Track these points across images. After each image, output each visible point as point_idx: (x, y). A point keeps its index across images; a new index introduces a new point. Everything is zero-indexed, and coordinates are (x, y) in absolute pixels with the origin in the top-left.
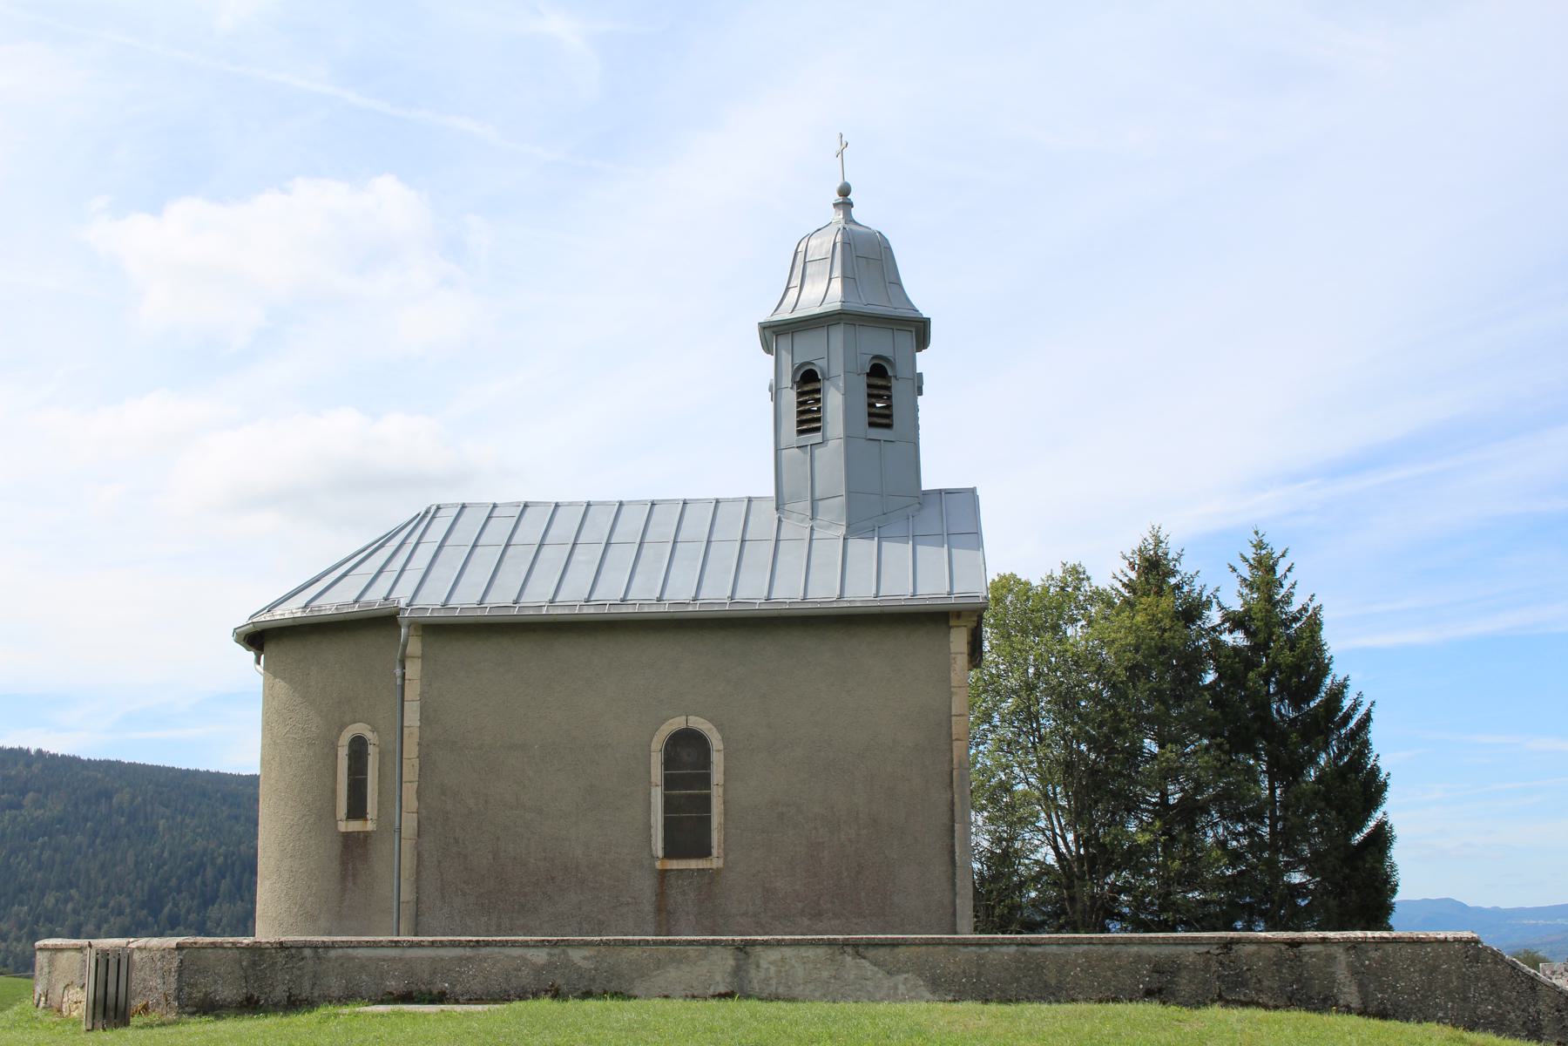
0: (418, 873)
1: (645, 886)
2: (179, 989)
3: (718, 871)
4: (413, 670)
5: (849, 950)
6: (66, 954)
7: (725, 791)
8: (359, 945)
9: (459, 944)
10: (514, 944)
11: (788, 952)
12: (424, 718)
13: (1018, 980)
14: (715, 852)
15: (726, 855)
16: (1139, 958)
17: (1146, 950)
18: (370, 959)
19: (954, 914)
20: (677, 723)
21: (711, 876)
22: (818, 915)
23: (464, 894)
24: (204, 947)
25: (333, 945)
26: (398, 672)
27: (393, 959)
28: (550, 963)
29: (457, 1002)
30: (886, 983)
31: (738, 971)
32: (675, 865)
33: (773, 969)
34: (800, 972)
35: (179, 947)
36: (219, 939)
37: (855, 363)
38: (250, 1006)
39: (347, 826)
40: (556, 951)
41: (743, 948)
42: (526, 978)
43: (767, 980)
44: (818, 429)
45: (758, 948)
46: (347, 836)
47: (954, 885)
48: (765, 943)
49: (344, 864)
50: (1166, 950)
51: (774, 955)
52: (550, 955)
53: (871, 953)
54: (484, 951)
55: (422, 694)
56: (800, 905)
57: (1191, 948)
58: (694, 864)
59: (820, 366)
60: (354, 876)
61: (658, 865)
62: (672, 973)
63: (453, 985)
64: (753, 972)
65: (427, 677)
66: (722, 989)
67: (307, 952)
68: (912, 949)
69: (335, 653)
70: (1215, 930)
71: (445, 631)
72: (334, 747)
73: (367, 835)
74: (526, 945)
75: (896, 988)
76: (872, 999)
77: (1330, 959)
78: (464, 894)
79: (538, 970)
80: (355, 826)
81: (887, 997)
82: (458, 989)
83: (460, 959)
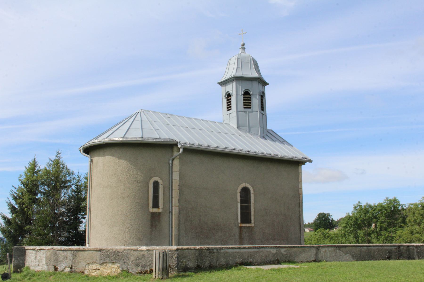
0: (179, 226)
1: (237, 230)
3: (253, 227)
4: (176, 162)
6: (86, 253)
8: (230, 248)
9: (255, 248)
10: (268, 247)
11: (326, 249)
14: (252, 222)
15: (255, 223)
16: (386, 249)
18: (232, 252)
19: (301, 240)
21: (251, 228)
22: (274, 240)
23: (192, 233)
24: (185, 249)
26: (171, 162)
27: (238, 253)
28: (276, 253)
29: (254, 265)
31: (316, 254)
33: (323, 254)
35: (177, 250)
36: (189, 247)
37: (249, 92)
38: (198, 269)
39: (152, 210)
40: (278, 249)
41: (318, 248)
42: (271, 257)
44: (250, 108)
46: (153, 213)
47: (301, 232)
48: (323, 247)
49: (152, 222)
52: (276, 250)
55: (180, 170)
59: (231, 92)
60: (155, 226)
61: (239, 225)
63: (253, 260)
64: (319, 254)
65: (181, 164)
66: (313, 259)
67: (215, 251)
68: (349, 248)
69: (147, 154)
71: (190, 151)
72: (148, 184)
73: (160, 213)
74: (271, 248)
77: (414, 249)
78: (192, 233)
79: (274, 255)
80: (155, 210)
81: (345, 260)
82: (255, 261)
83: (255, 252)
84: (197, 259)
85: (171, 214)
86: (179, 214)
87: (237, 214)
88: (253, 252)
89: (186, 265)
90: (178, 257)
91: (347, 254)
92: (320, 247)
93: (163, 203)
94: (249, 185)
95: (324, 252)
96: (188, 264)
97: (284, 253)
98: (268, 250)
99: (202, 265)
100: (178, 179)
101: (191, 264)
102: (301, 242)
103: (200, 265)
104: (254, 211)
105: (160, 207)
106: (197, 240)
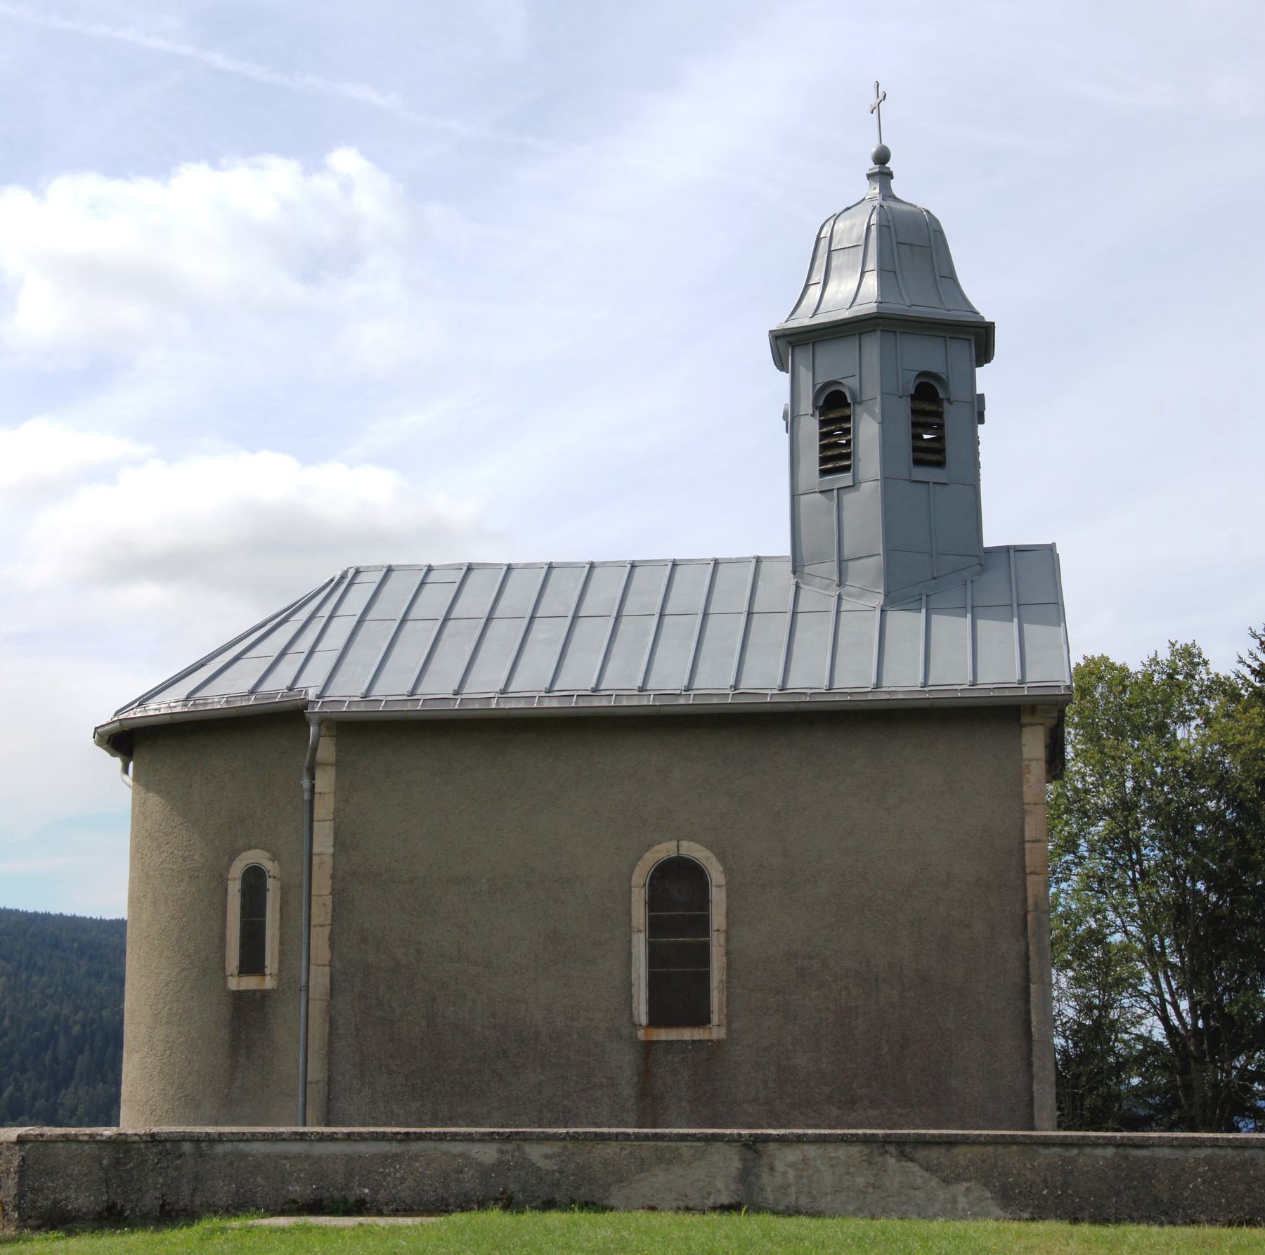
0: (331, 1043)
1: (624, 1062)
3: (719, 1043)
4: (325, 781)
5: (891, 1149)
7: (728, 939)
9: (383, 1137)
10: (454, 1137)
11: (812, 1151)
12: (341, 844)
14: (715, 1018)
15: (729, 1023)
18: (268, 1156)
19: (1031, 1104)
21: (711, 1049)
25: (221, 1138)
26: (306, 783)
27: (296, 1157)
29: (380, 1213)
31: (746, 1176)
32: (663, 1035)
33: (791, 1174)
35: (21, 1141)
37: (895, 379)
39: (234, 984)
40: (509, 1147)
41: (752, 1146)
43: (784, 1188)
44: (846, 469)
45: (772, 1146)
46: (239, 996)
47: (1030, 1064)
48: (781, 1139)
51: (793, 1154)
52: (501, 1152)
53: (921, 1154)
54: (415, 1147)
55: (336, 812)
56: (826, 1090)
58: (687, 1034)
61: (641, 1035)
64: (765, 1178)
65: (344, 790)
66: (725, 1199)
67: (187, 1147)
71: (374, 733)
72: (223, 881)
73: (265, 994)
74: (469, 1138)
76: (923, 1215)
79: (485, 1172)
80: (250, 983)
82: (382, 1196)
83: (385, 1156)
84: (107, 1181)
85: (303, 993)
86: (331, 996)
87: (630, 986)
88: (373, 1156)
89: (55, 1202)
90: (23, 1171)
91: (958, 1179)
92: (767, 1139)
93: (282, 953)
94: (697, 846)
95: (793, 1165)
96: (68, 1198)
97: (542, 1163)
98: (458, 1148)
99: (129, 1206)
100: (331, 850)
101: (80, 1200)
102: (1031, 1117)
103: (120, 1203)
104: (729, 967)
105: (267, 971)
106: (415, 1105)
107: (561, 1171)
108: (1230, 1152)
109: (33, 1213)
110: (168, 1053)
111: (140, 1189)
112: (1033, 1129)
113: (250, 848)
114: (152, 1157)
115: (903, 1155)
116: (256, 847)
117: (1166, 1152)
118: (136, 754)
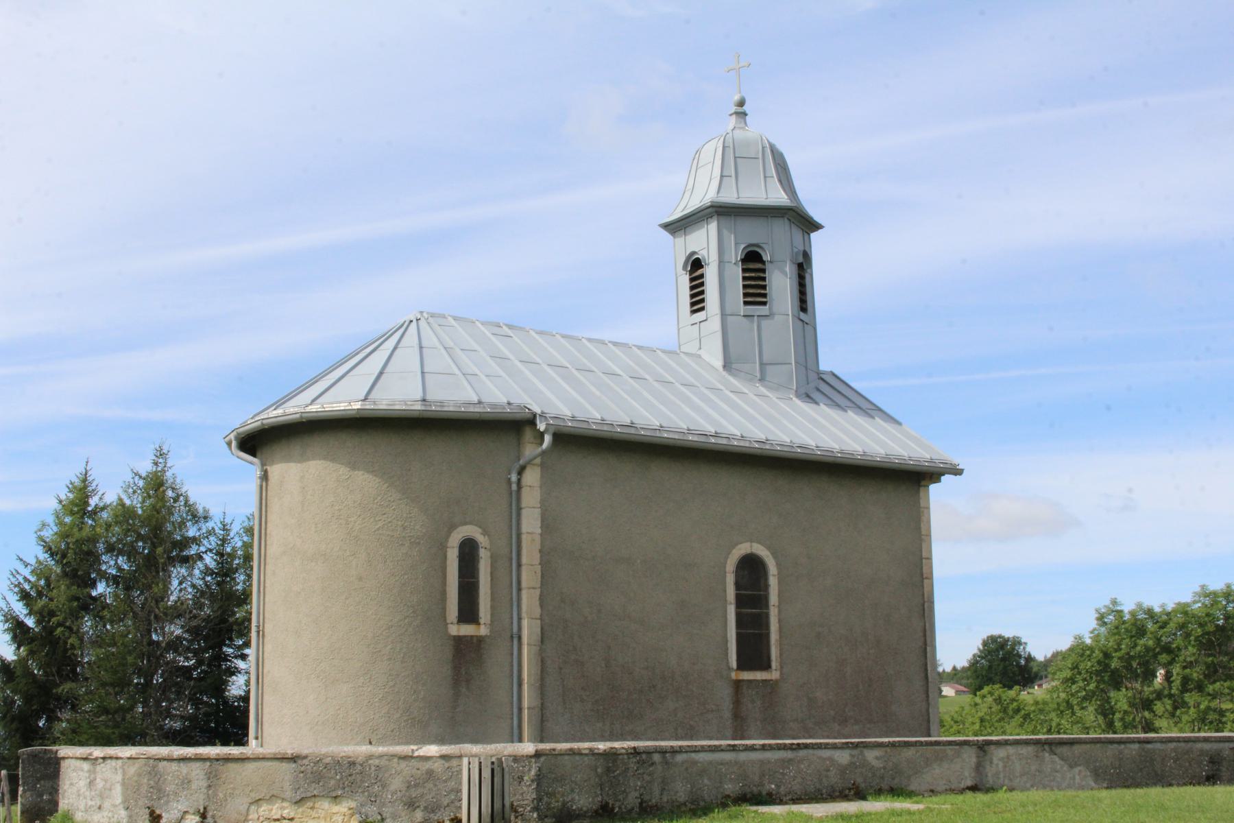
0: (542, 679)
1: (724, 694)
2: (539, 799)
3: (777, 681)
4: (532, 477)
5: (1046, 747)
7: (780, 612)
13: (1141, 770)
14: (774, 664)
15: (782, 667)
17: (1207, 746)
18: (710, 763)
19: (929, 721)
20: (743, 549)
22: (844, 721)
25: (680, 750)
26: (514, 478)
27: (728, 763)
29: (781, 802)
30: (1069, 775)
31: (979, 767)
32: (747, 676)
34: (1018, 767)
36: (575, 745)
37: (760, 252)
39: (456, 630)
40: (855, 752)
41: (983, 747)
42: (834, 778)
43: (997, 774)
44: (764, 303)
45: (993, 747)
46: (458, 640)
49: (457, 668)
50: (1216, 746)
51: (1001, 753)
52: (852, 756)
53: (1060, 750)
54: (802, 753)
55: (543, 502)
56: (832, 713)
57: (1227, 745)
60: (468, 681)
61: (733, 675)
62: (937, 770)
65: (548, 485)
66: (969, 783)
67: (657, 757)
69: (439, 452)
70: (711, 739)
71: (575, 441)
72: (443, 548)
73: (480, 640)
74: (835, 747)
75: (1074, 778)
79: (843, 770)
80: (467, 630)
82: (782, 790)
83: (783, 760)
84: (601, 786)
86: (542, 642)
88: (776, 761)
89: (564, 804)
90: (539, 779)
91: (1076, 765)
93: (493, 607)
96: (573, 799)
97: (876, 763)
99: (617, 804)
100: (539, 531)
103: (611, 802)
105: (482, 621)
106: (599, 725)
107: (884, 768)
108: (1183, 744)
109: (549, 813)
110: (391, 684)
111: (624, 791)
112: (929, 736)
113: (466, 524)
114: (633, 766)
115: (1053, 752)
116: (470, 523)
117: (1158, 746)
118: (258, 454)
